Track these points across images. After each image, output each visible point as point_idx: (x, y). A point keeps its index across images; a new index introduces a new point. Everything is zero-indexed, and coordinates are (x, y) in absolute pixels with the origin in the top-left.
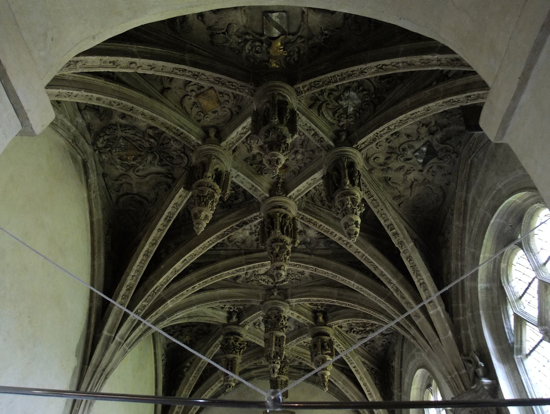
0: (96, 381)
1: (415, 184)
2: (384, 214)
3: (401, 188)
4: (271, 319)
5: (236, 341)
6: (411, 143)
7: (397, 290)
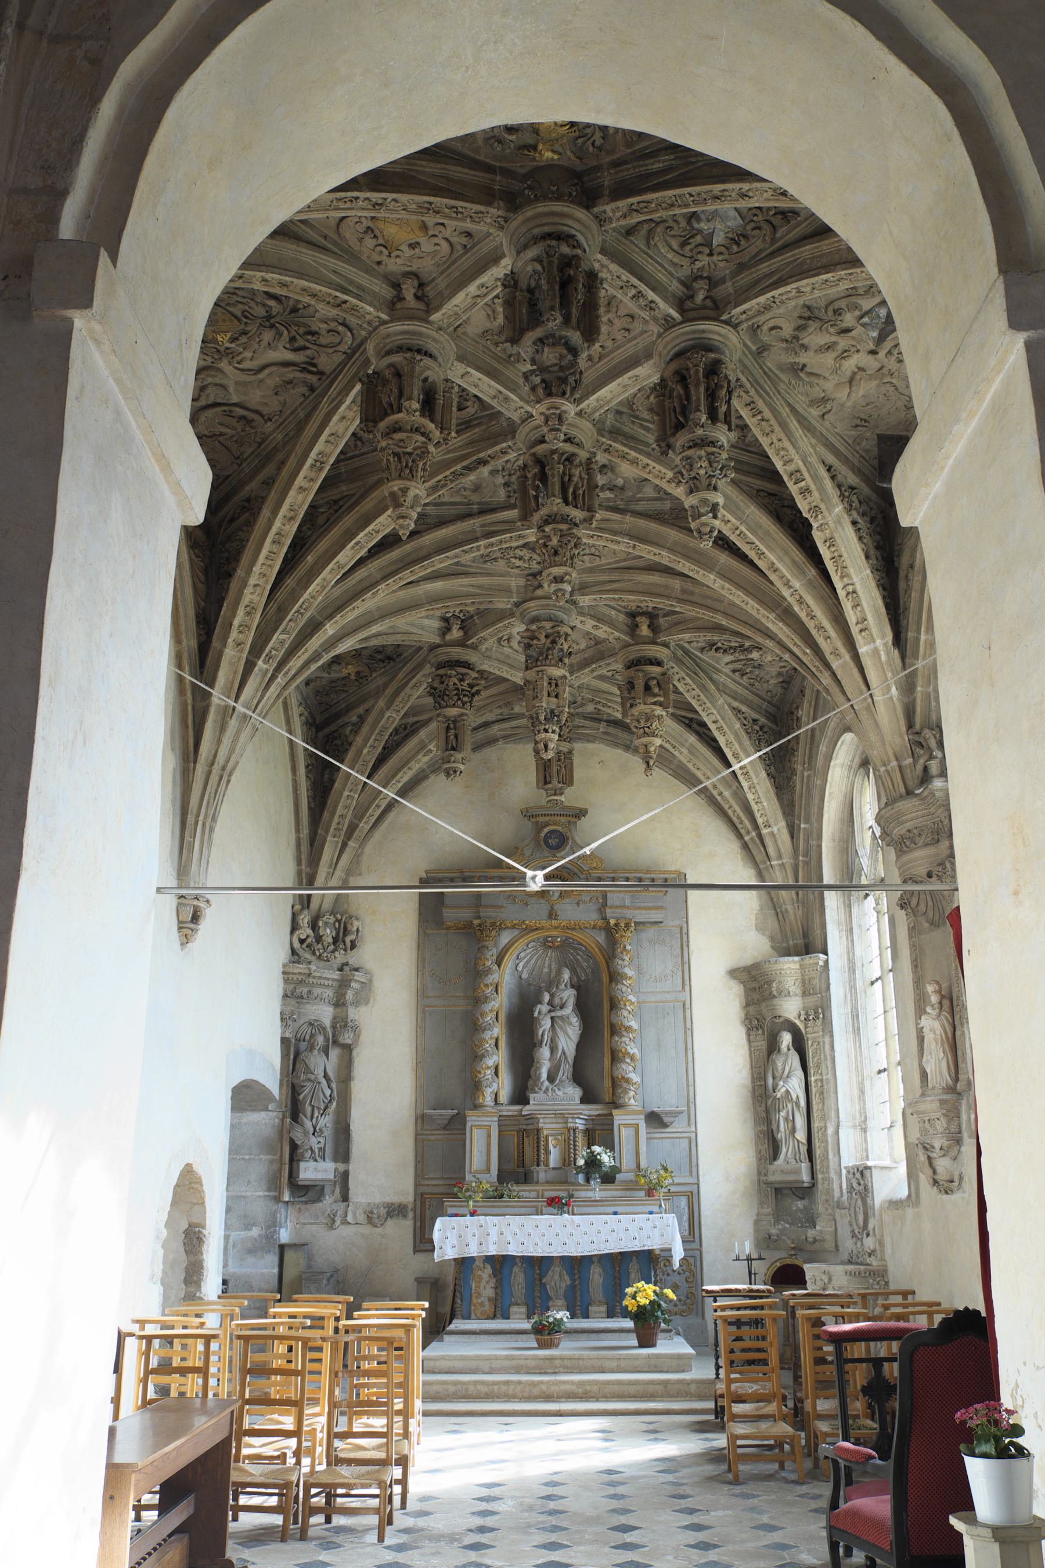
0: (214, 790)
1: (858, 377)
2: (783, 449)
3: (829, 386)
4: (539, 640)
5: (461, 680)
6: (853, 299)
7: (801, 601)
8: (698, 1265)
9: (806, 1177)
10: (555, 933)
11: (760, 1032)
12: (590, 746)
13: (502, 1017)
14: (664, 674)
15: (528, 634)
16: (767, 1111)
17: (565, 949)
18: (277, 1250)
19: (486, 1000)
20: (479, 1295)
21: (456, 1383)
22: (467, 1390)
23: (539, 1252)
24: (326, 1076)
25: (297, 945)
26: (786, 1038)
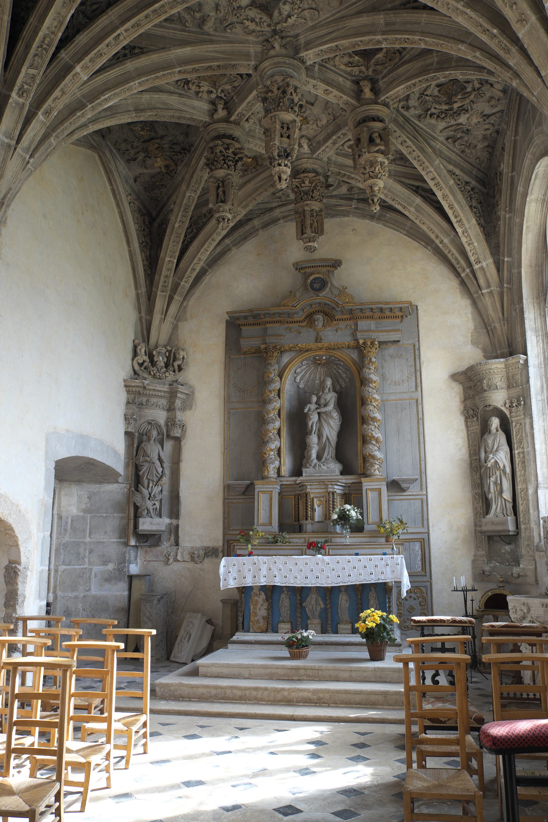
4: (272, 92)
5: (228, 149)
8: (429, 593)
9: (511, 527)
10: (320, 353)
11: (475, 419)
12: (346, 219)
13: (284, 414)
14: (384, 129)
15: (265, 90)
16: (481, 478)
17: (328, 364)
18: (126, 579)
19: (270, 401)
20: (256, 614)
21: (216, 687)
22: (225, 693)
23: (299, 583)
24: (160, 459)
25: (137, 367)
26: (495, 422)
